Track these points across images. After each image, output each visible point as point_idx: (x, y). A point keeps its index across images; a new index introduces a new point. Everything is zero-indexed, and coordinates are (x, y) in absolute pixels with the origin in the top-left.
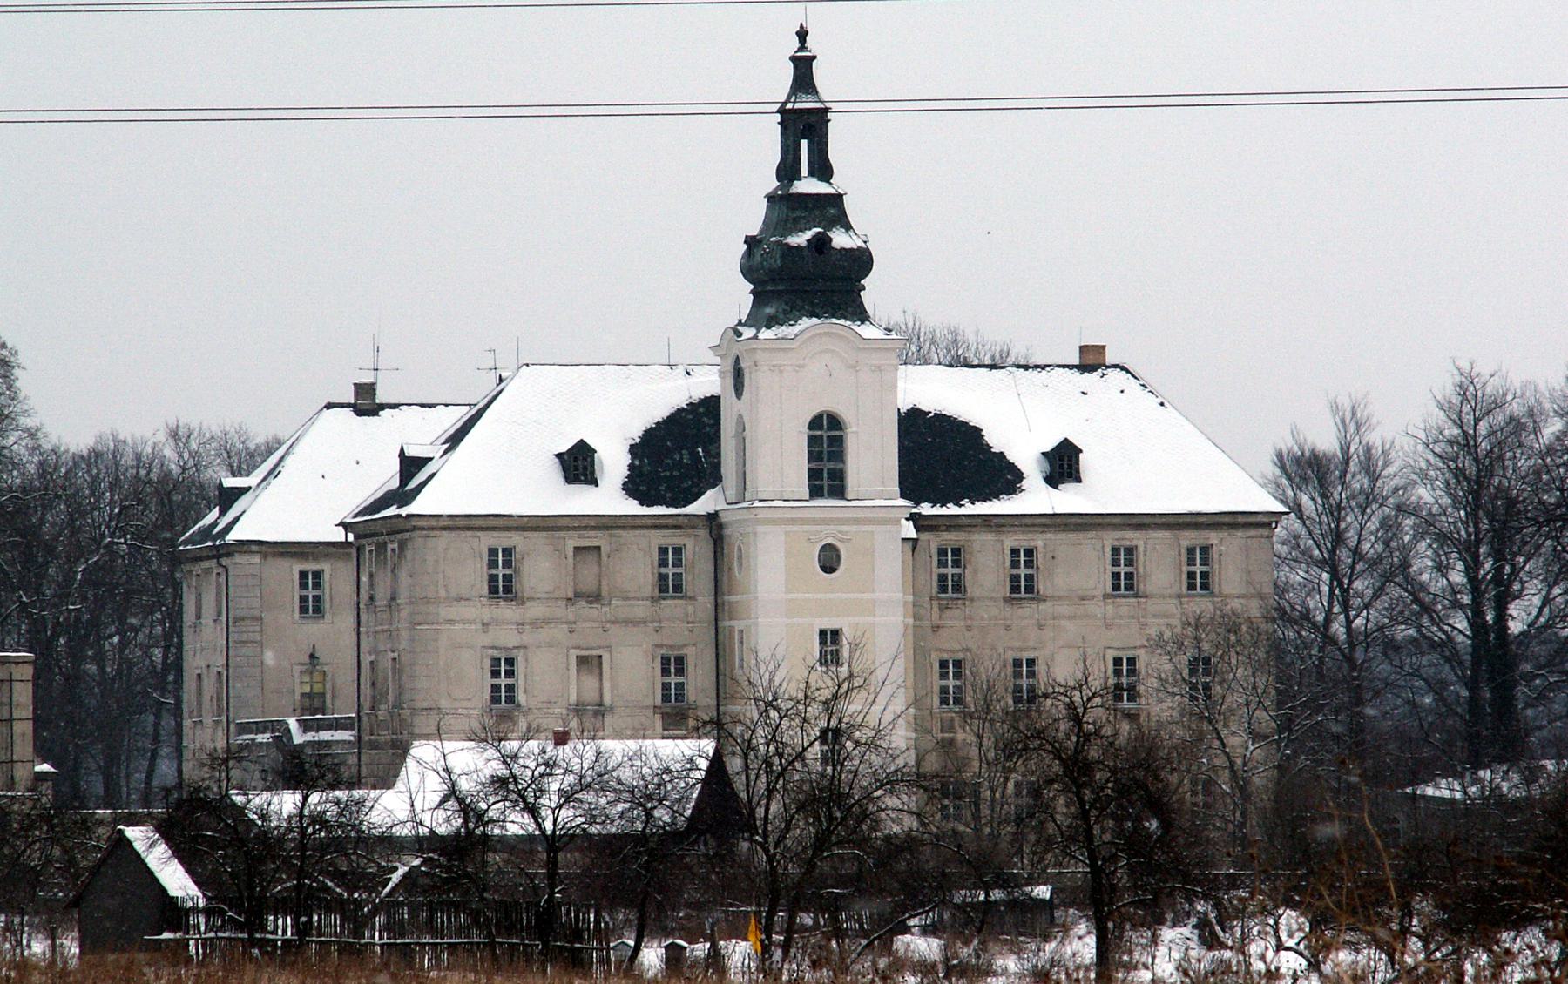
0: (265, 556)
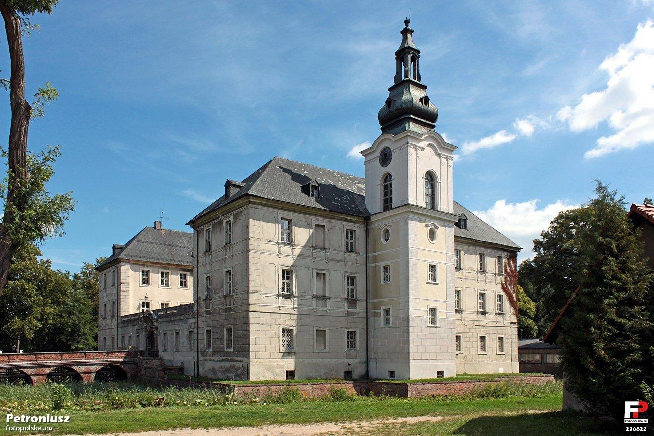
0: (293, 179)
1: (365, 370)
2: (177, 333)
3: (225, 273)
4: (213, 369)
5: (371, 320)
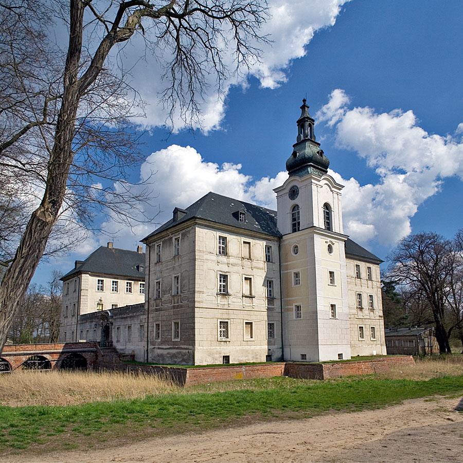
1: (281, 354)
2: (129, 327)
3: (173, 278)
4: (162, 355)
5: (285, 314)
